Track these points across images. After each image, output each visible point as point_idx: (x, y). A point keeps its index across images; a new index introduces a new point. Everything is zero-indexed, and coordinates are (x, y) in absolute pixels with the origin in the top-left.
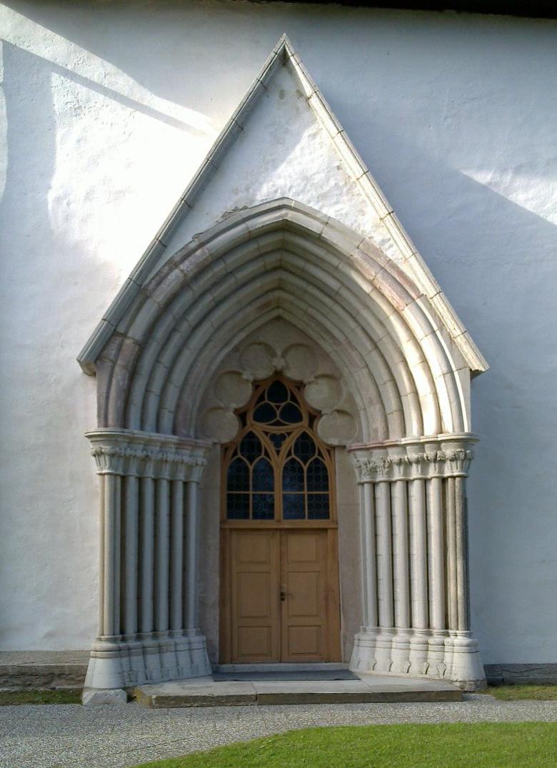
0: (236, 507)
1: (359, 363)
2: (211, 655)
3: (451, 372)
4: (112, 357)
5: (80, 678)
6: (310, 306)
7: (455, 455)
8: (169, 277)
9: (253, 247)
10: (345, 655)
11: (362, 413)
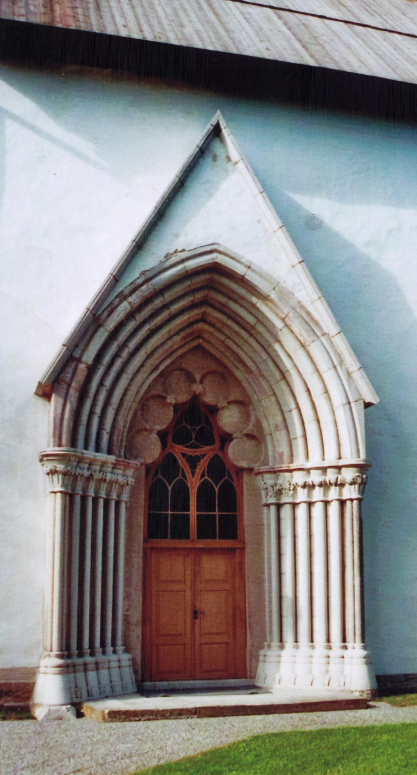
0: (155, 528)
1: (267, 390)
2: (136, 672)
3: (349, 403)
4: (67, 380)
5: (27, 695)
6: (228, 337)
7: (354, 479)
8: (119, 308)
9: (187, 283)
10: (251, 671)
11: (268, 439)
